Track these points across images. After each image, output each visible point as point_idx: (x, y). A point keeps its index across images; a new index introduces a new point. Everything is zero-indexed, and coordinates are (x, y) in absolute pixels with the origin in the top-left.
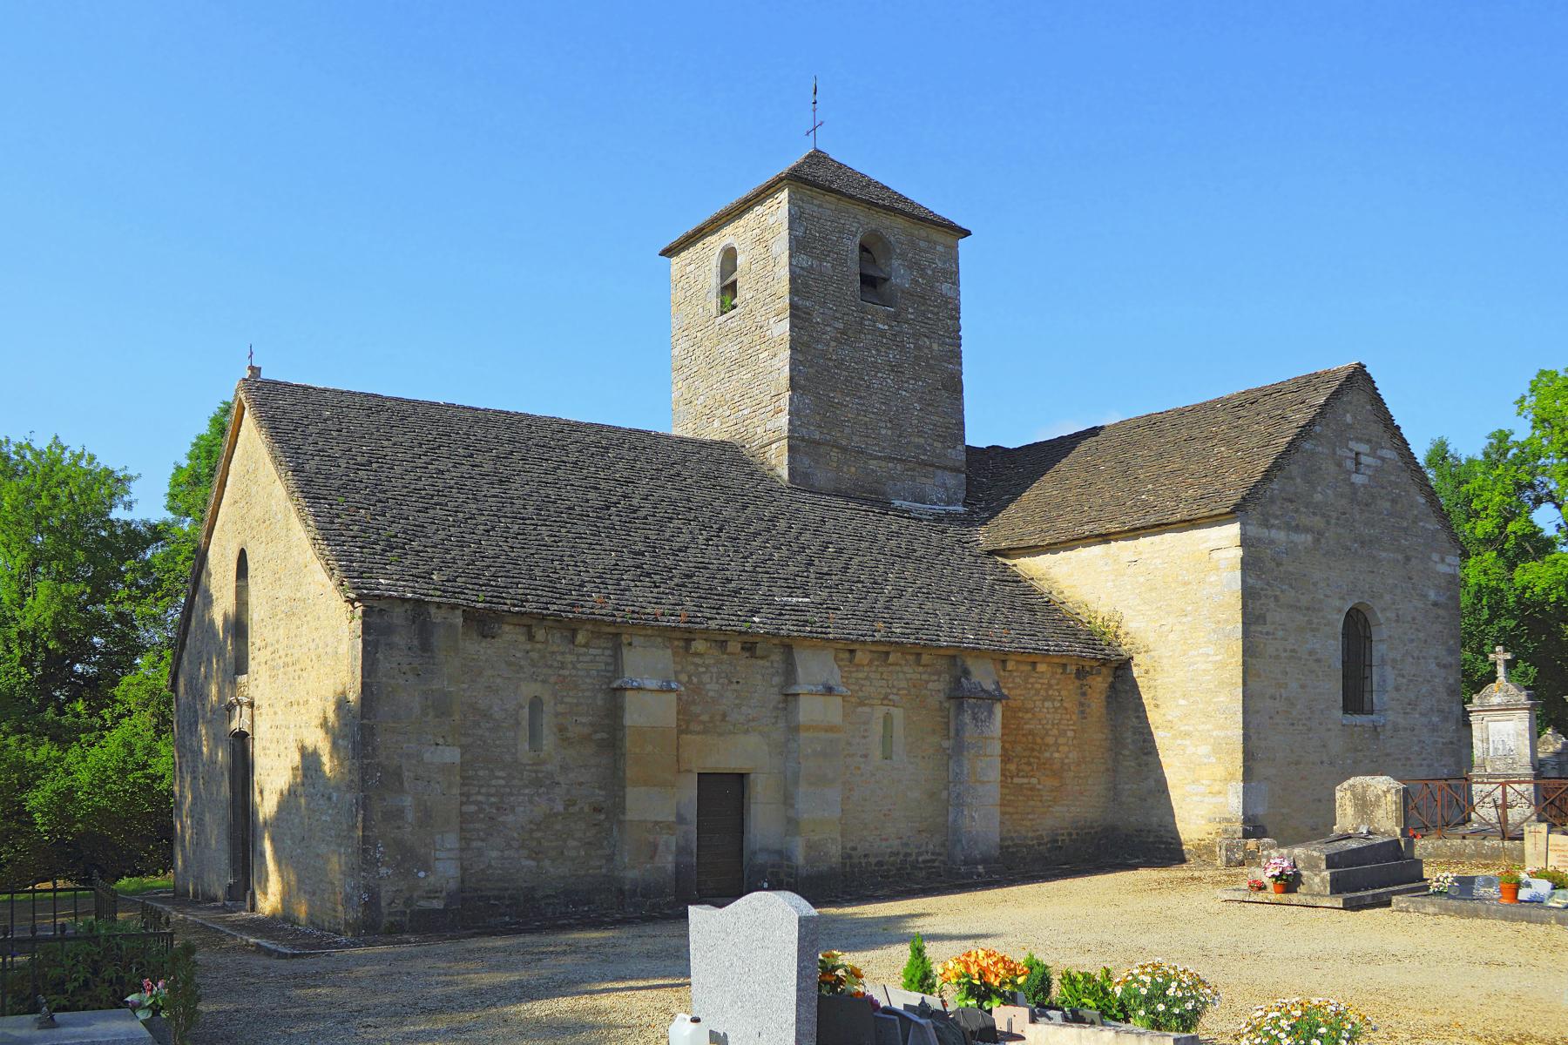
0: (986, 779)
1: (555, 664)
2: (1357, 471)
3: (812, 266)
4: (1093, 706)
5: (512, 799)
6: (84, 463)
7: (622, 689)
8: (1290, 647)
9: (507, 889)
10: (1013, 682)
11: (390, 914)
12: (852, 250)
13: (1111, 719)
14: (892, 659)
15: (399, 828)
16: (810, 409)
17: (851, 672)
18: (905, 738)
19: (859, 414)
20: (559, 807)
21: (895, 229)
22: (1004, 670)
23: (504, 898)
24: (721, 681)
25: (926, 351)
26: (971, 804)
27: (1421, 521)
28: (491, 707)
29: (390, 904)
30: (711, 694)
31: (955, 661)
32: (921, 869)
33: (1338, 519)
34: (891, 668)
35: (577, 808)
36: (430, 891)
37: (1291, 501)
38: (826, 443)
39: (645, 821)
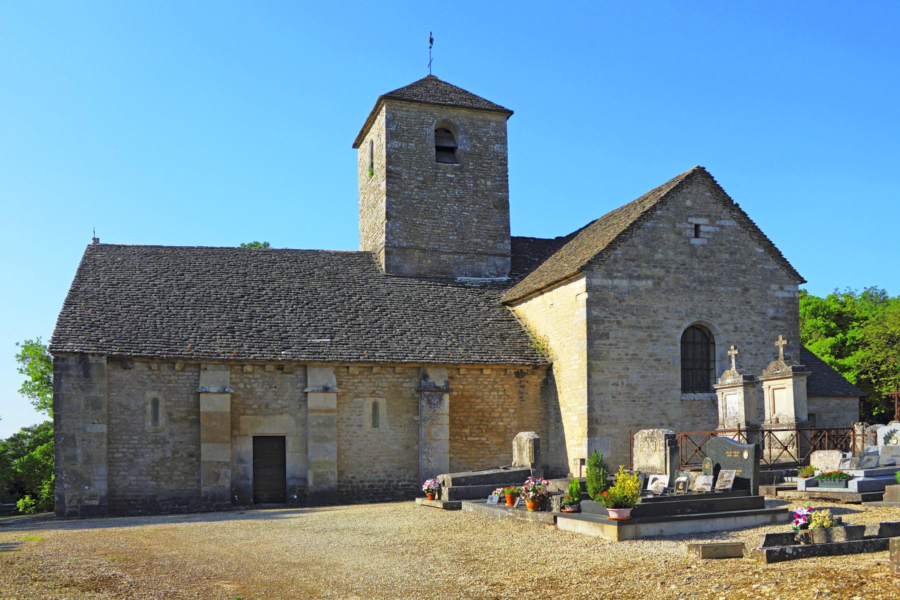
0: (438, 438)
1: (166, 381)
2: (697, 236)
3: (401, 146)
4: (530, 393)
5: (142, 450)
6: (378, 265)
7: (199, 393)
8: (632, 352)
9: (140, 496)
10: (467, 381)
11: (70, 507)
12: (429, 134)
13: (545, 401)
14: (374, 370)
15: (74, 465)
16: (399, 229)
17: (349, 379)
18: (387, 415)
19: (433, 229)
20: (169, 454)
21: (459, 117)
22: (459, 374)
23: (138, 500)
24: (265, 386)
25: (482, 187)
26: (428, 452)
27: (759, 264)
28: (129, 404)
29: (70, 502)
30: (259, 394)
31: (421, 370)
32: (401, 489)
33: (677, 268)
34: (376, 376)
35: (179, 455)
36: (91, 496)
37: (633, 260)
38: (411, 247)
39: (212, 461)
